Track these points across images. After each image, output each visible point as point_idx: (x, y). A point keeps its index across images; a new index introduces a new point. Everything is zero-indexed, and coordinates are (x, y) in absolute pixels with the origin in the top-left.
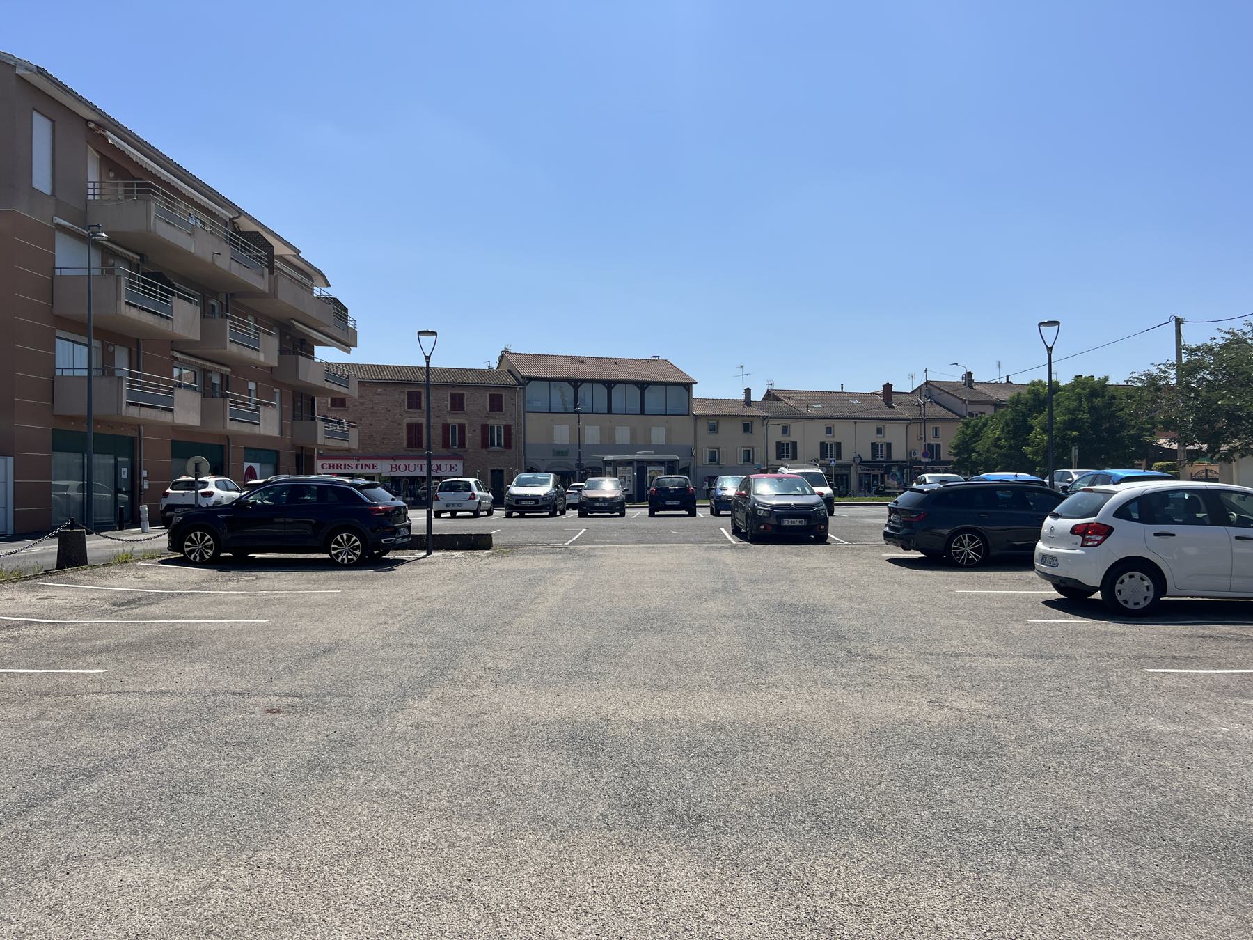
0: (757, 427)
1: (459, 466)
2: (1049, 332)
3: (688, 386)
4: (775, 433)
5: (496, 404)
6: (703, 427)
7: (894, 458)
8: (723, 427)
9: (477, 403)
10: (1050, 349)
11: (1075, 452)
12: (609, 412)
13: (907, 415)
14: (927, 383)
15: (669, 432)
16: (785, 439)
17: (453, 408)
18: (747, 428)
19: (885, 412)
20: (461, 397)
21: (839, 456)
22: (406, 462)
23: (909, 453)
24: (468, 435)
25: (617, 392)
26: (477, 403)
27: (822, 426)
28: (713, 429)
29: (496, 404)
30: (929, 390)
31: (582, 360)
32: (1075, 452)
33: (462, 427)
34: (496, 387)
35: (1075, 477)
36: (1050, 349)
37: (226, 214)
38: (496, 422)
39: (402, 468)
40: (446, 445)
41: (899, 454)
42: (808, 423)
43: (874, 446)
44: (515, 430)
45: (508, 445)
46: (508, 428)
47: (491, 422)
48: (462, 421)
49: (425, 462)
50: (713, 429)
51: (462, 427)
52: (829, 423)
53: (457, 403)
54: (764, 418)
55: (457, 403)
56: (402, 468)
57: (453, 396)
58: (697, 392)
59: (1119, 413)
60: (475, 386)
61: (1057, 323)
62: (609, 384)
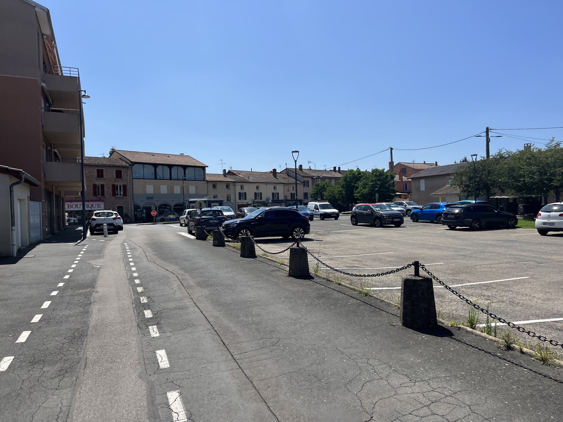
0: (231, 186)
1: (102, 205)
2: (295, 155)
3: (204, 168)
4: (238, 189)
5: (119, 175)
6: (211, 186)
7: (280, 199)
8: (218, 186)
9: (110, 174)
10: (296, 161)
11: (377, 195)
12: (171, 179)
13: (283, 182)
14: (286, 169)
15: (197, 188)
16: (242, 191)
17: (98, 176)
18: (227, 186)
19: (273, 179)
20: (102, 171)
21: (261, 198)
22: (76, 203)
23: (285, 197)
24: (106, 190)
25: (174, 170)
26: (110, 174)
27: (255, 186)
28: (214, 186)
29: (119, 175)
30: (287, 171)
31: (153, 155)
32: (377, 195)
33: (103, 186)
34: (119, 167)
35: (246, 211)
36: (296, 161)
37: (47, 32)
38: (119, 183)
39: (74, 206)
40: (95, 194)
41: (281, 197)
42: (250, 185)
43: (273, 194)
44: (128, 187)
45: (125, 194)
46: (125, 187)
47: (116, 183)
48: (102, 183)
49: (81, 203)
50: (214, 186)
51: (103, 186)
52: (257, 184)
53: (100, 174)
54: (234, 182)
55: (100, 174)
56: (74, 206)
57: (98, 171)
58: (208, 171)
59: (498, 167)
60: (110, 166)
61: (298, 152)
62: (170, 166)
